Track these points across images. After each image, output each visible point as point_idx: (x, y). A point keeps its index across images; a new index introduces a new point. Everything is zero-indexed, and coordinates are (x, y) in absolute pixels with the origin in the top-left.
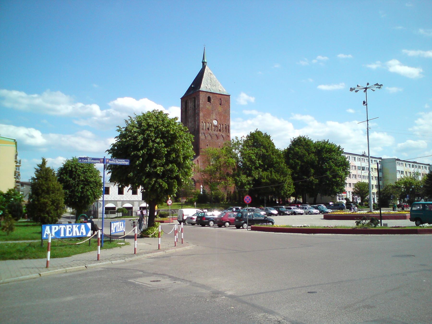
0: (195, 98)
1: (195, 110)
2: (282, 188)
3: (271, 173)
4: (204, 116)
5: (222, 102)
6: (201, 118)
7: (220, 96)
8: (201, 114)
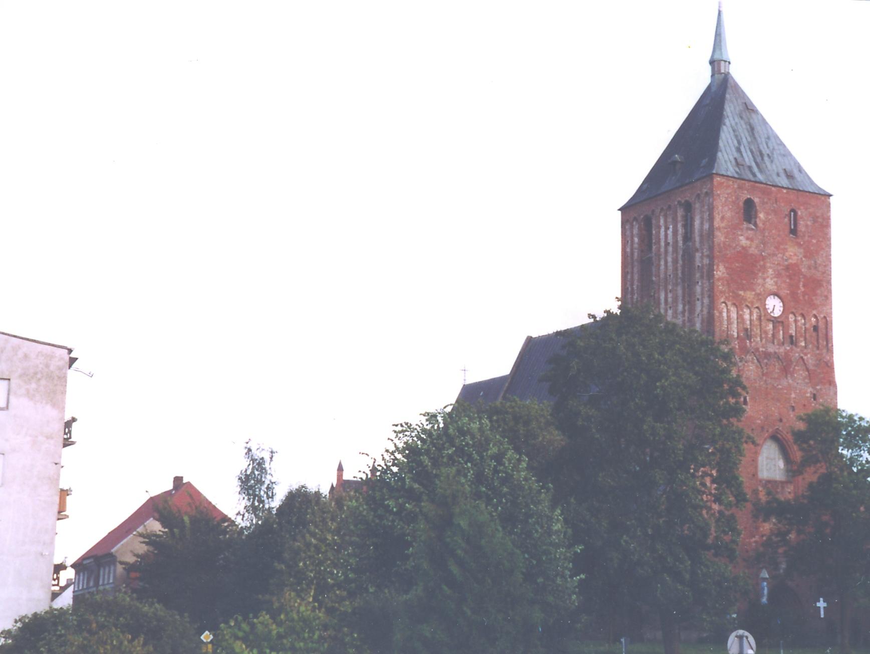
0: (688, 207)
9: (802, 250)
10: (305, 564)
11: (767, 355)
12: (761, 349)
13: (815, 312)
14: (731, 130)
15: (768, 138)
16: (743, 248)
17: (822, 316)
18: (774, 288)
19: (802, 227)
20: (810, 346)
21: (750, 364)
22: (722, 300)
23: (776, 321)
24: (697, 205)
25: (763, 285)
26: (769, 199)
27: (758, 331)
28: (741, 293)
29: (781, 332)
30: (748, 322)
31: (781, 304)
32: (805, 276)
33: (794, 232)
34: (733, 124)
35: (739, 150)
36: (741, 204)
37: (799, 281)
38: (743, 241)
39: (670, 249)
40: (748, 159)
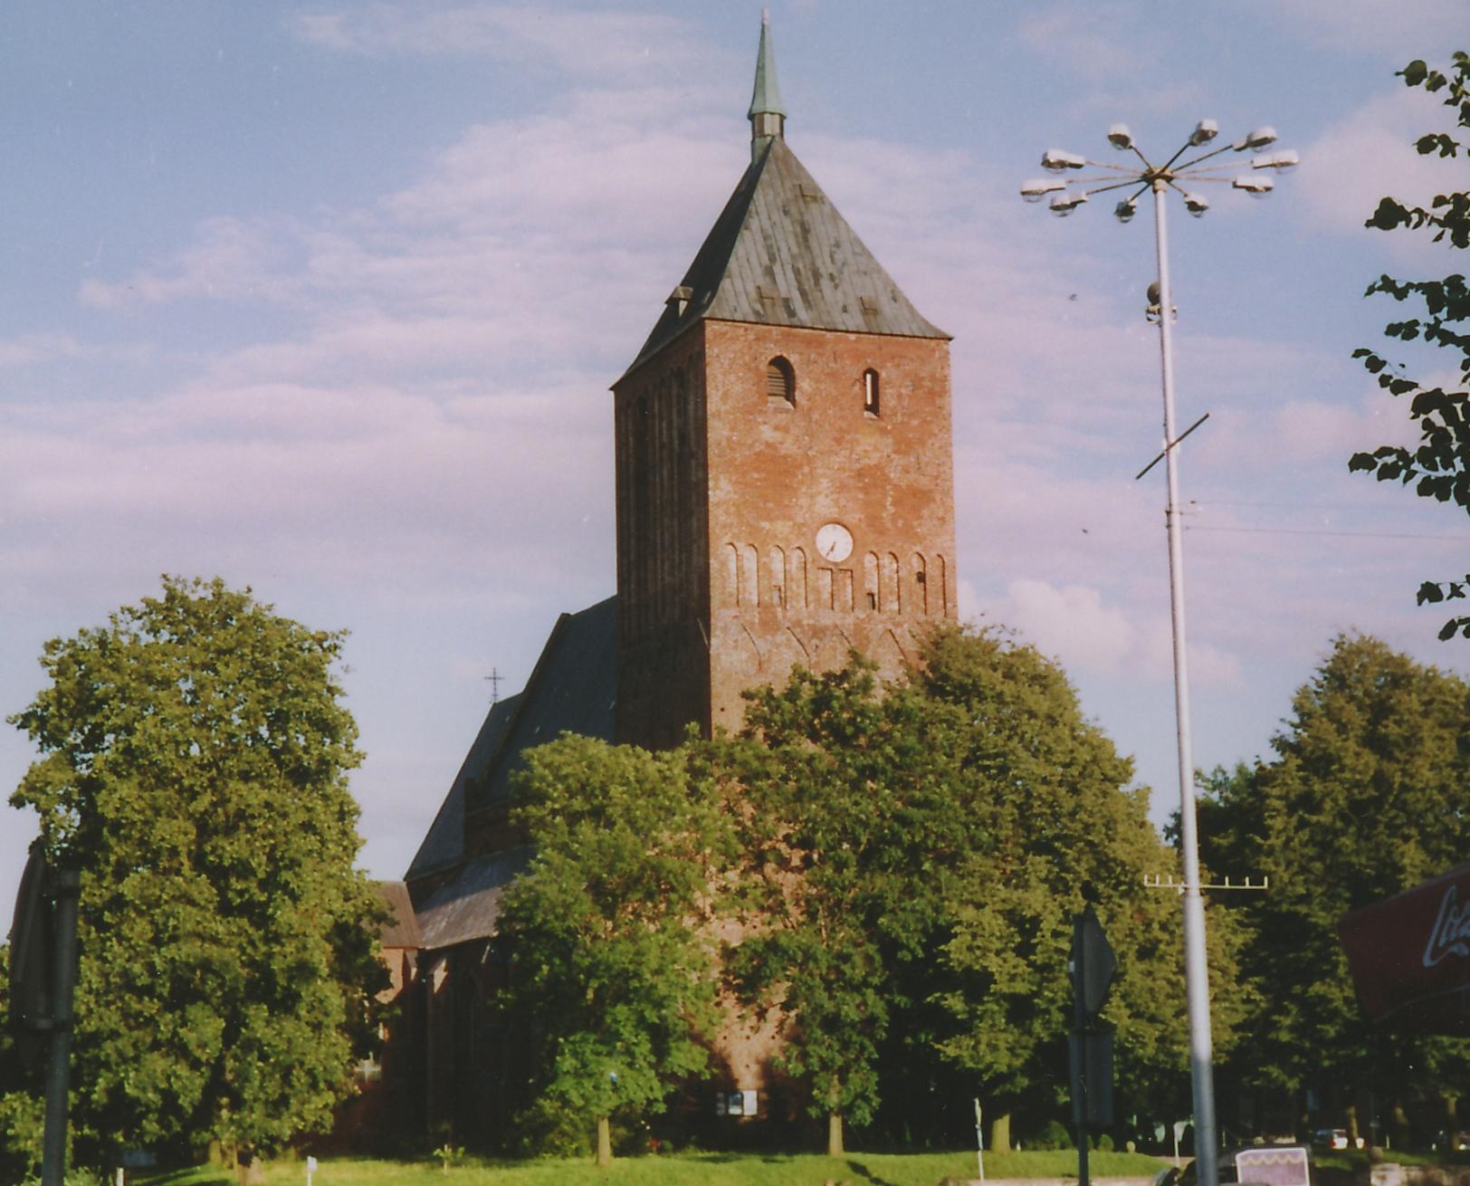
9: (890, 440)
11: (818, 632)
12: (805, 622)
13: (918, 549)
14: (759, 238)
15: (837, 245)
16: (768, 445)
17: (934, 554)
18: (833, 512)
19: (888, 399)
20: (909, 609)
21: (783, 649)
22: (727, 539)
23: (836, 570)
25: (810, 508)
26: (821, 355)
27: (802, 591)
29: (849, 589)
30: (781, 576)
31: (850, 539)
32: (896, 487)
33: (874, 408)
34: (767, 224)
35: (769, 272)
36: (764, 367)
37: (885, 495)
38: (767, 433)
39: (665, 453)
40: (786, 285)
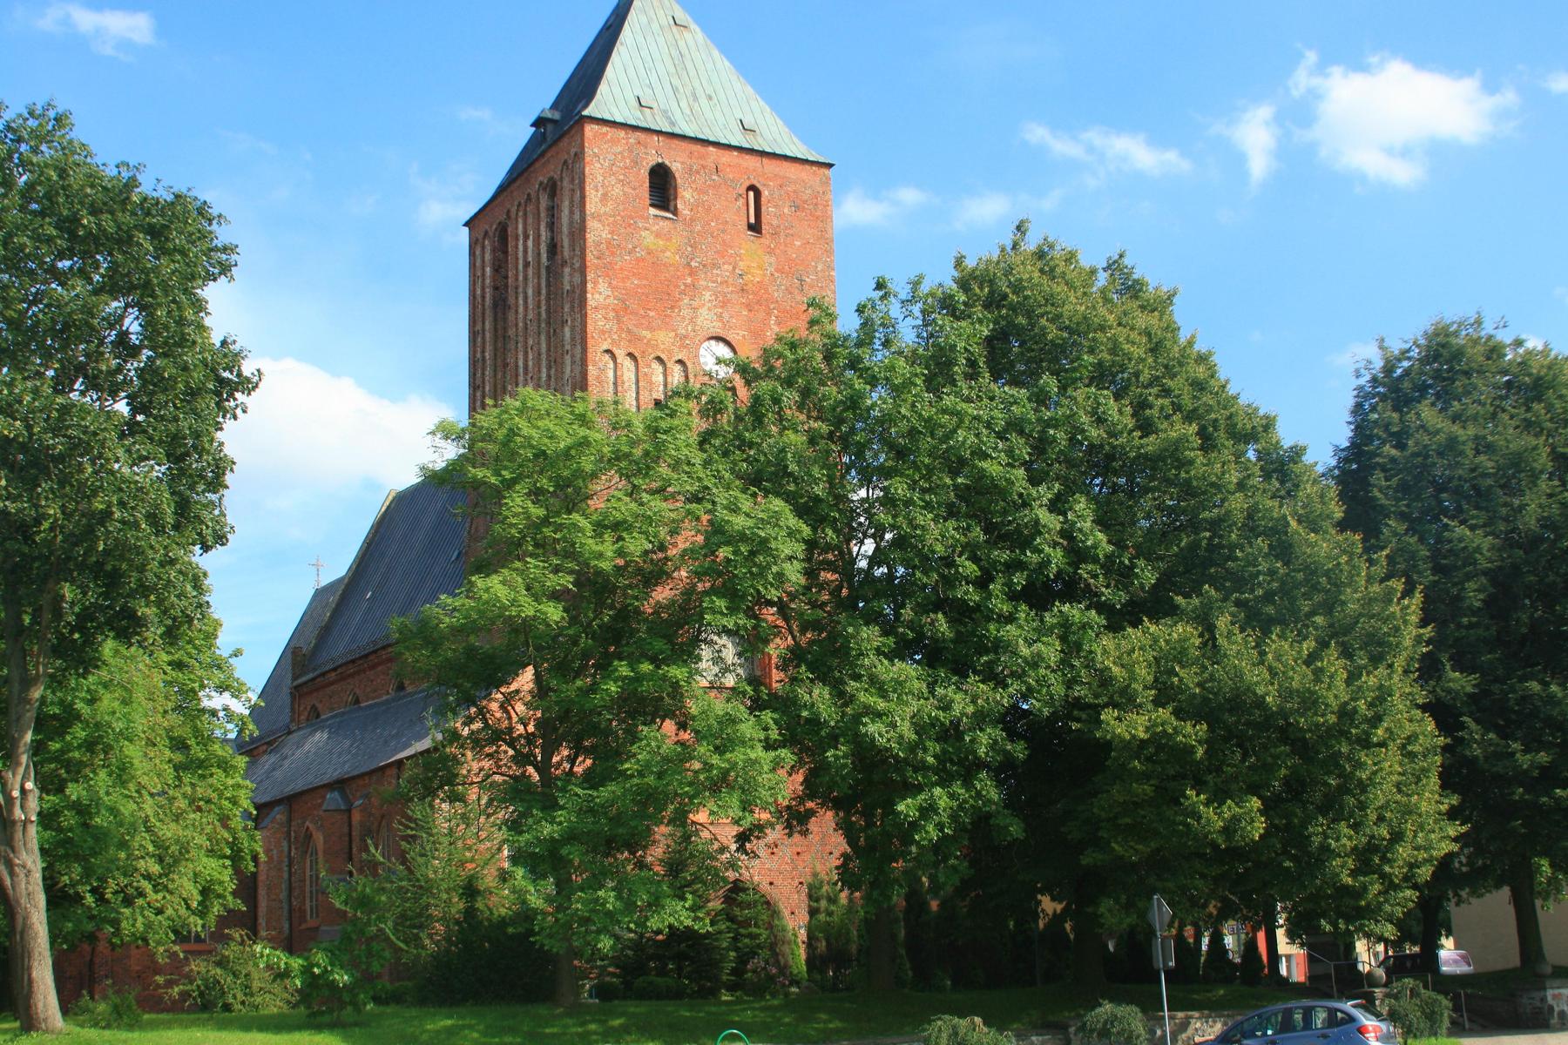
1: (553, 272)
2: (1342, 799)
3: (1209, 629)
4: (621, 311)
5: (768, 210)
6: (597, 322)
7: (751, 162)
8: (599, 294)
10: (1294, 858)
24: (566, 183)
28: (646, 334)
33: (755, 228)
38: (648, 239)
